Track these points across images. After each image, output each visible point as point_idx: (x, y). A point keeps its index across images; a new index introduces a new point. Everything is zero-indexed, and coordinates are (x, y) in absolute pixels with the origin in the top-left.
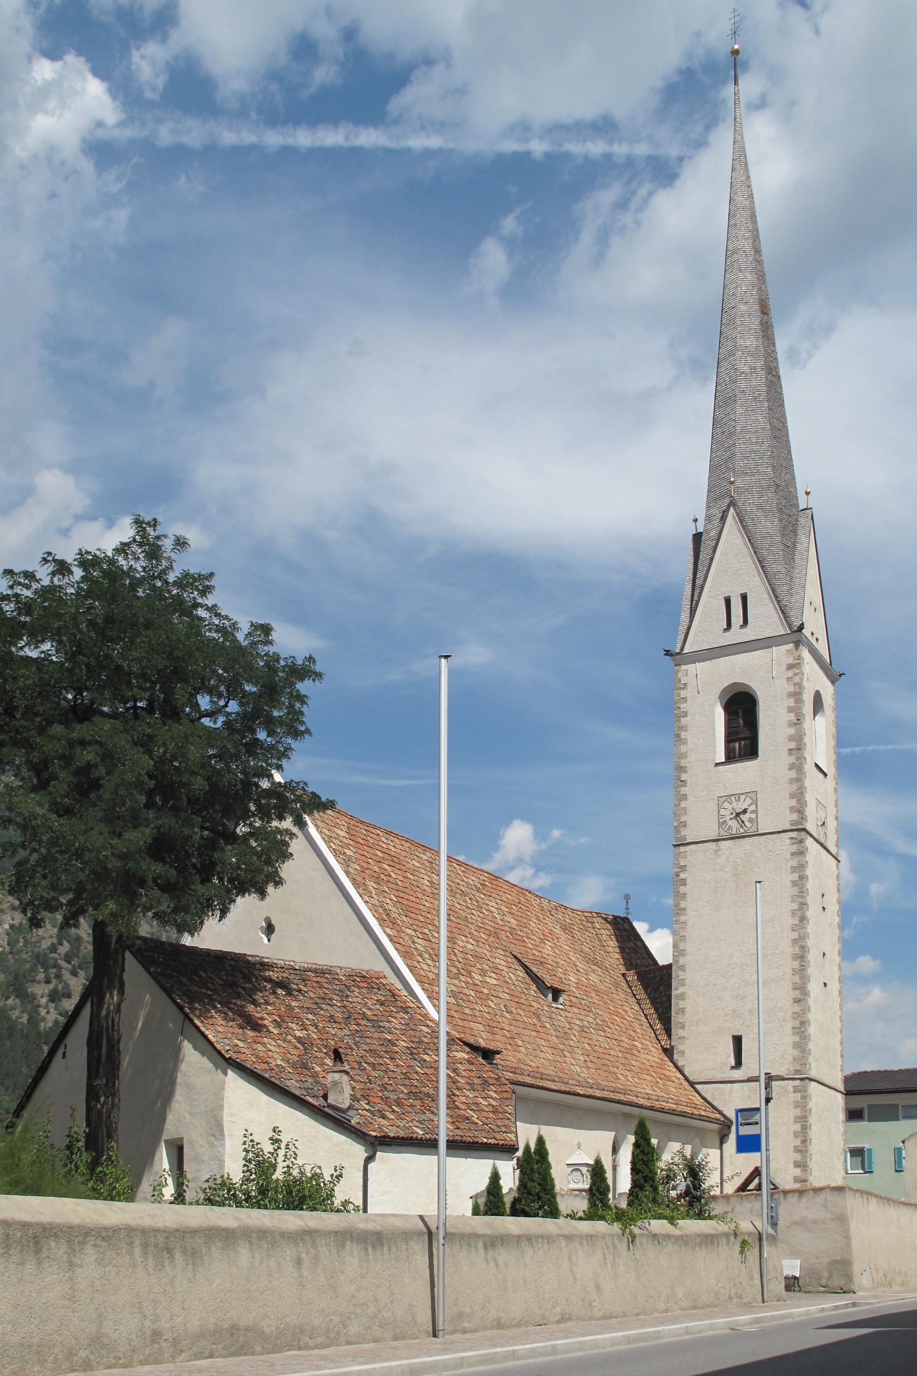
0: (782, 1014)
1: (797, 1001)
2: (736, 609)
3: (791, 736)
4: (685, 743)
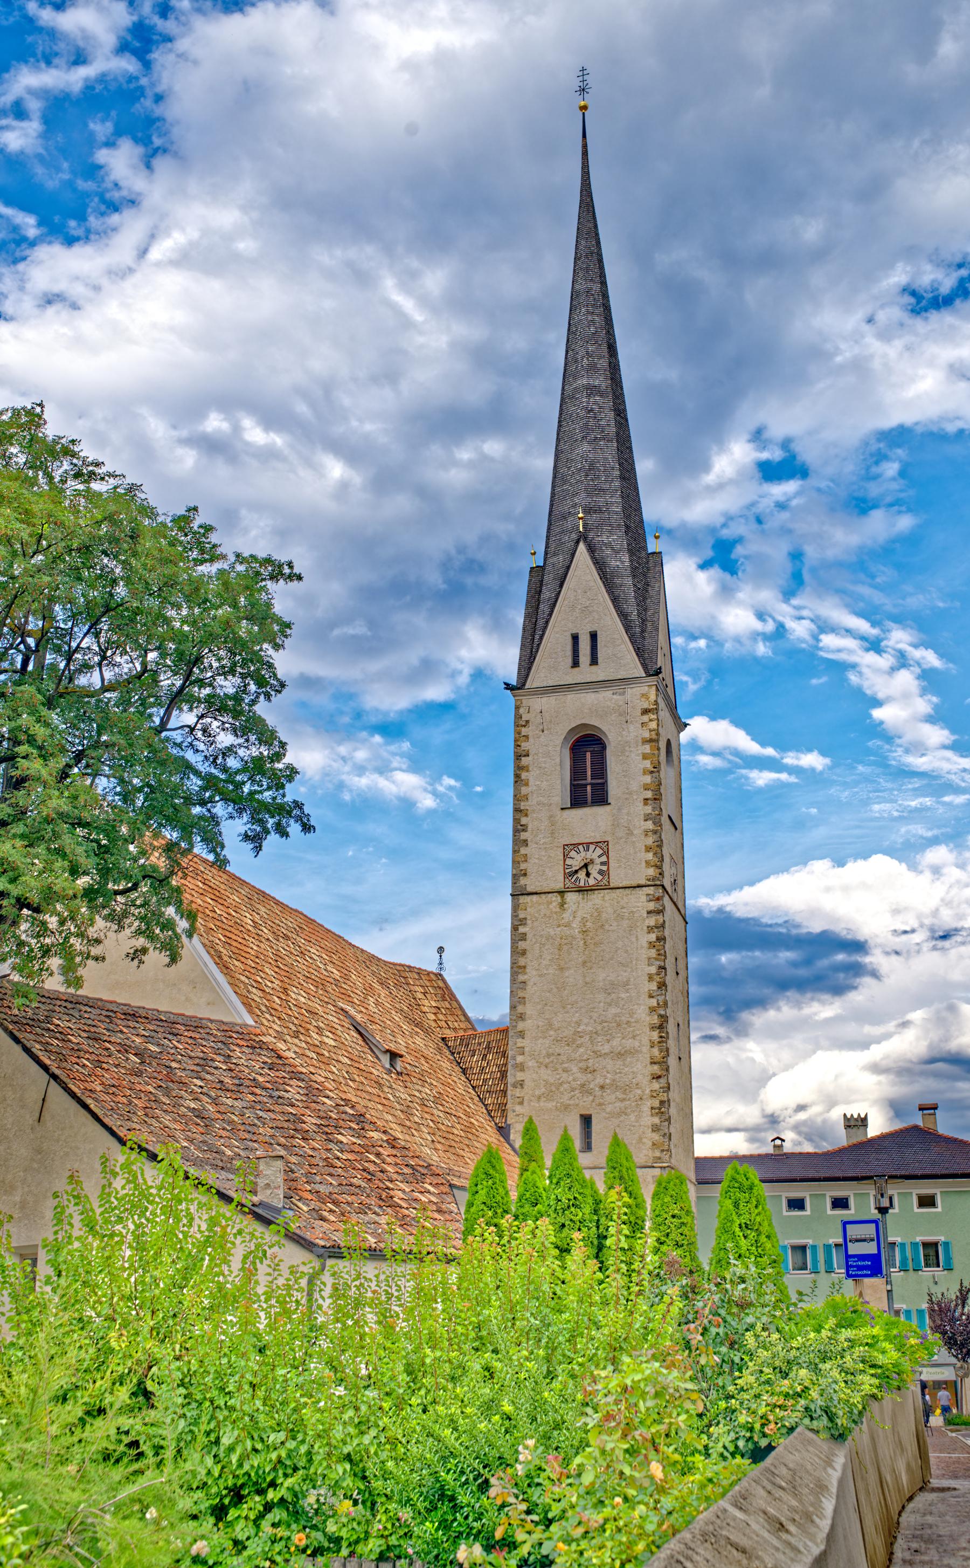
0: (639, 1092)
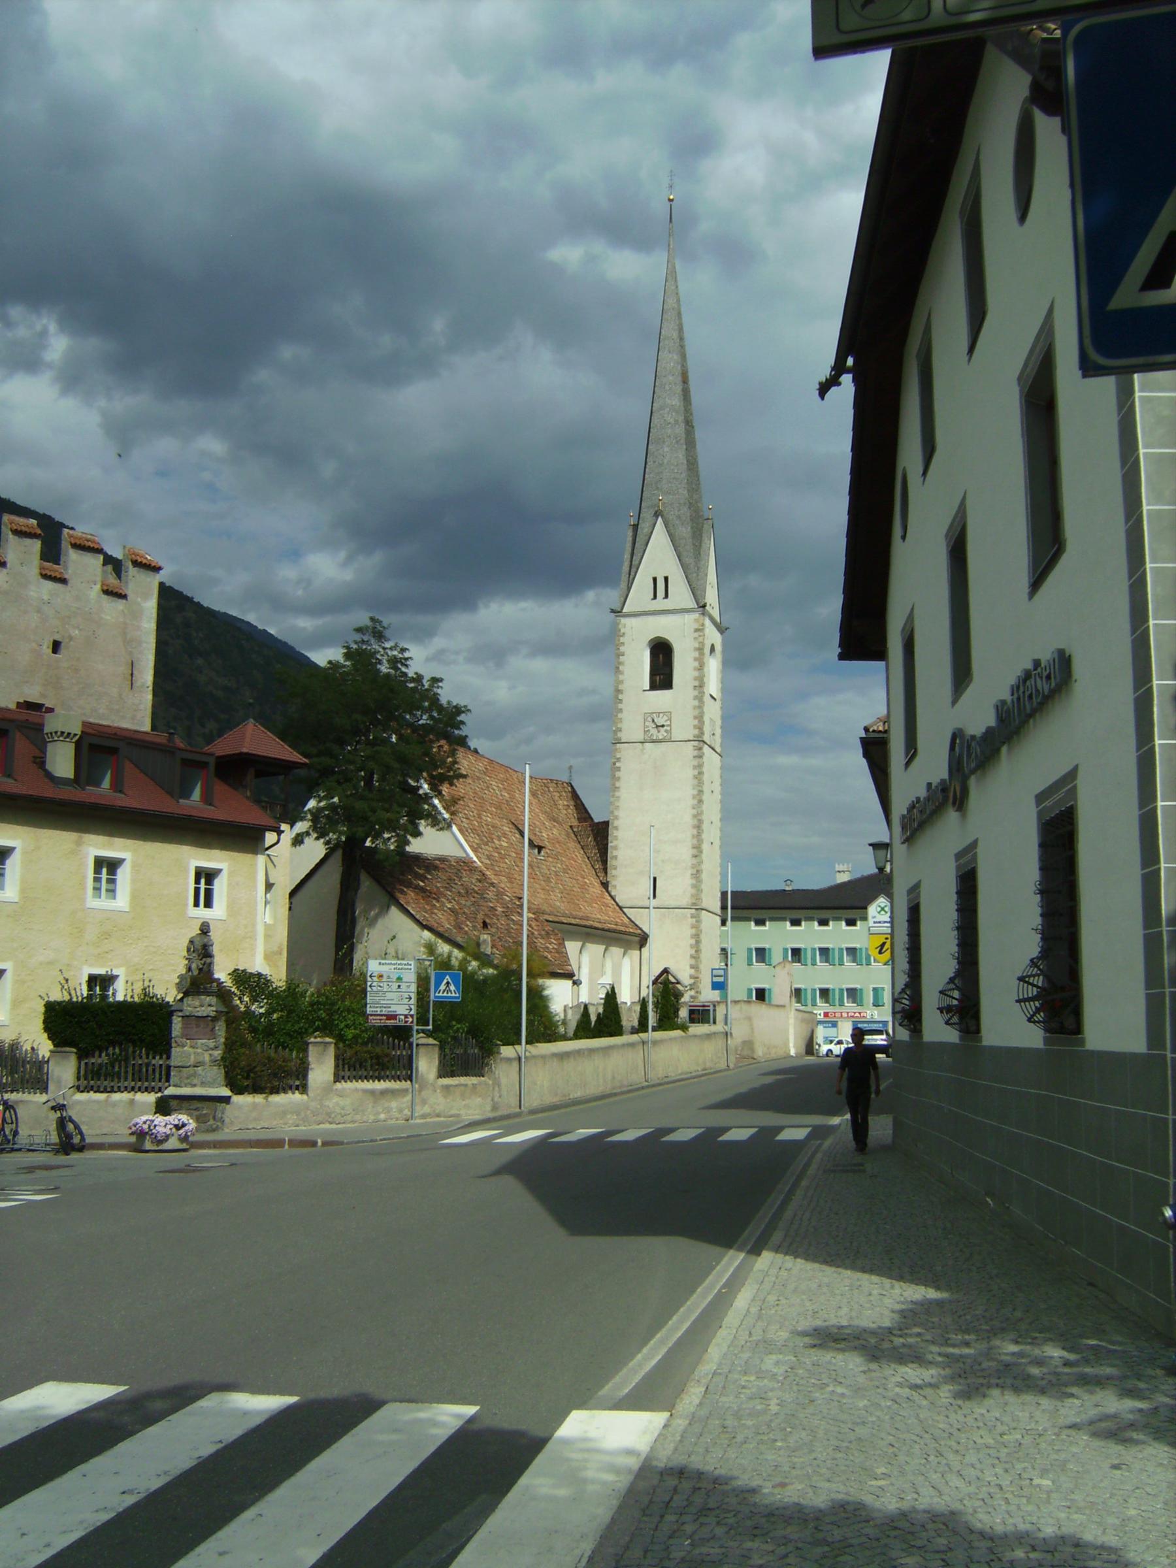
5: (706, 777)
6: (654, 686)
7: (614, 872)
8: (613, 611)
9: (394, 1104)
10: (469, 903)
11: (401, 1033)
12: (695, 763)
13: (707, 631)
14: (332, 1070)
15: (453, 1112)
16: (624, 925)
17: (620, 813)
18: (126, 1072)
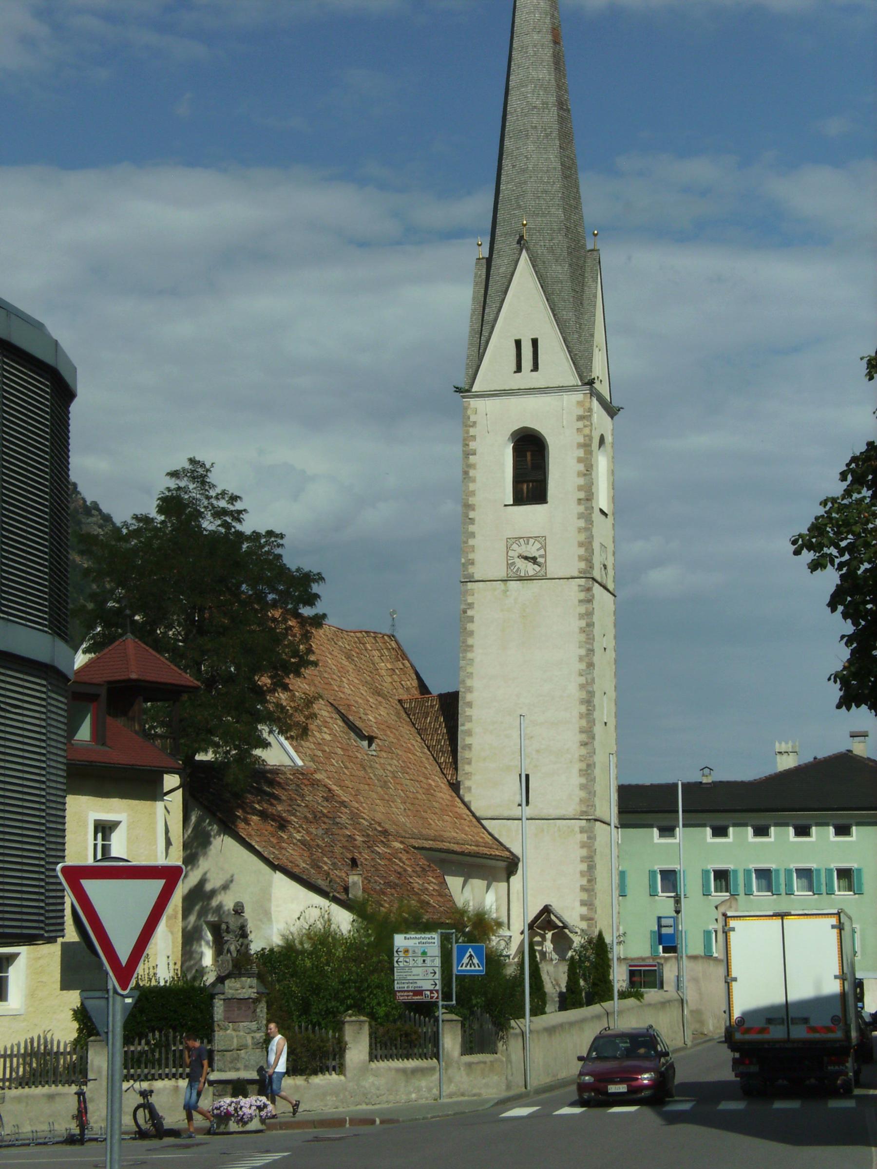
1: (584, 744)
2: (528, 354)
3: (581, 486)
4: (474, 481)
5: (597, 631)
6: (519, 499)
7: (467, 768)
8: (458, 390)
9: (423, 1083)
10: (320, 832)
11: (426, 1009)
12: (582, 609)
13: (595, 416)
14: (367, 1049)
15: (476, 1091)
16: (486, 845)
17: (475, 683)
18: (167, 1059)
